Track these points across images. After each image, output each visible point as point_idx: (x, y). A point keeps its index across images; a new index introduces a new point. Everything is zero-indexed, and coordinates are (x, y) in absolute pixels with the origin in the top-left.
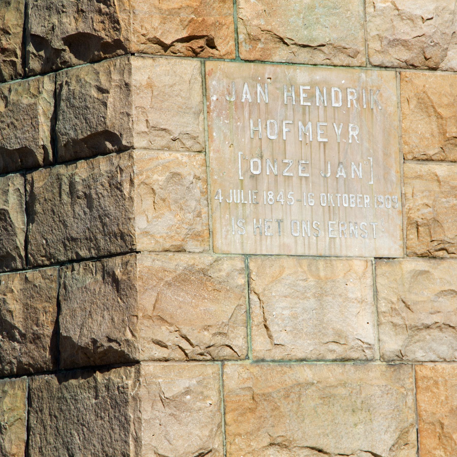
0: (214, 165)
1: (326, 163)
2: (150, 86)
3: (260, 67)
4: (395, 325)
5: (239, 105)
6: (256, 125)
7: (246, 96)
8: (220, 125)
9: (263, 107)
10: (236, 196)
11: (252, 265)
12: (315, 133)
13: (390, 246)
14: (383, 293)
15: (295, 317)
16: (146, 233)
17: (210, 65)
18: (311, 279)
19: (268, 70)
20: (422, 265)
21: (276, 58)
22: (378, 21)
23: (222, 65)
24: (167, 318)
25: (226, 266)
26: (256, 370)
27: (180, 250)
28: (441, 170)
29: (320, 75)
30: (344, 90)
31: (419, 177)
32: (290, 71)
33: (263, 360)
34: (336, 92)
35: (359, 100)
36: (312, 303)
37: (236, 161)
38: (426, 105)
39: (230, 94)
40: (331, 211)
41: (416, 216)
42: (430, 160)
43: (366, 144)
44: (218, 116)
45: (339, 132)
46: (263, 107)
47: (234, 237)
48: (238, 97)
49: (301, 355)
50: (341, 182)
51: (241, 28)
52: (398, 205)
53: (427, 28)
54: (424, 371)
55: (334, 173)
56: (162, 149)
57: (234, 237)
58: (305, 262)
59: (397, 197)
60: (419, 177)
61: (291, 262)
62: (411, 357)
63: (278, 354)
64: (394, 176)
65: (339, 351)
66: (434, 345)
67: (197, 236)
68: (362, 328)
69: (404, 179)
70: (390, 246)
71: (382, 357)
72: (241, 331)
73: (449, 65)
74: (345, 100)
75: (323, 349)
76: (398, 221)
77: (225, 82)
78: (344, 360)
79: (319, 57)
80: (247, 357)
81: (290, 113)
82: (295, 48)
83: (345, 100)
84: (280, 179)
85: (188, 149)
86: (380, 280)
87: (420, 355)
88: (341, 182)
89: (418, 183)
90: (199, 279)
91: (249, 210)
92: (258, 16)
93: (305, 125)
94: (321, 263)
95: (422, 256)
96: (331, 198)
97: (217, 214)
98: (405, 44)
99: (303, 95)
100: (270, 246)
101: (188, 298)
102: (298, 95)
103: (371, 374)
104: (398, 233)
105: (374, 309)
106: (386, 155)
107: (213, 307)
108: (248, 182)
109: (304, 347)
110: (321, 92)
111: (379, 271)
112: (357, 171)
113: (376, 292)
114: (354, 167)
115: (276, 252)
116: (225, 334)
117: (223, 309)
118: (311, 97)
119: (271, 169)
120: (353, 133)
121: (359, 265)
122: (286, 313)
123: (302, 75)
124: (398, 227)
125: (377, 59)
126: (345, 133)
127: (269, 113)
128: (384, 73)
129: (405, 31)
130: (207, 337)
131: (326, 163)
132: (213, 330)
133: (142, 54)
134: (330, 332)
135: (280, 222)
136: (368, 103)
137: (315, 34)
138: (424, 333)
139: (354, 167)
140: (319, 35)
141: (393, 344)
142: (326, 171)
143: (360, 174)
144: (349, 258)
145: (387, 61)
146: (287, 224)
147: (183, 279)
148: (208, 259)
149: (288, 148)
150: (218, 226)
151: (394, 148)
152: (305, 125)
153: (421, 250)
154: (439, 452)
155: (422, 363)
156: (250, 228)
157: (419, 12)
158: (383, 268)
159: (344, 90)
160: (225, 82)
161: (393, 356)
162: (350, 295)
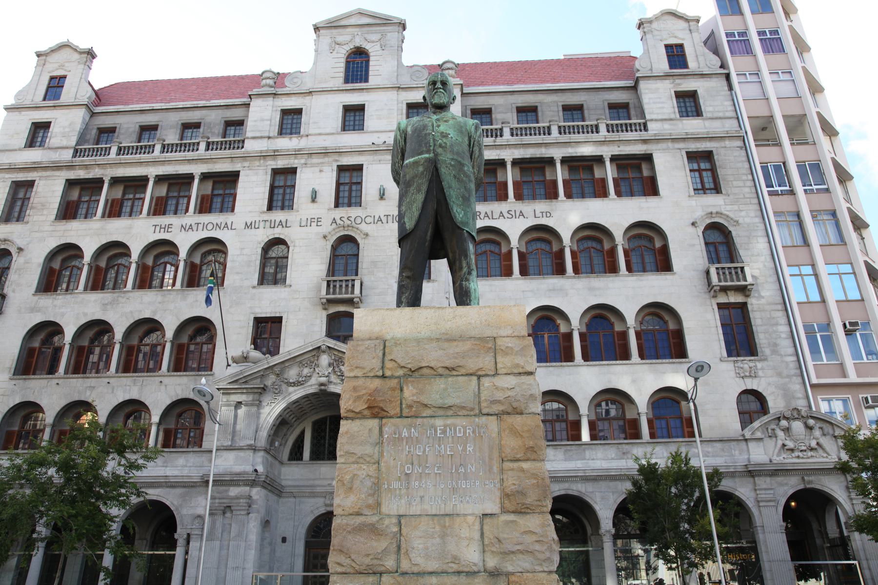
0: (383, 469)
1: (452, 465)
2: (346, 433)
3: (414, 420)
4: (493, 552)
5: (400, 439)
6: (410, 448)
7: (405, 433)
8: (388, 450)
9: (414, 439)
10: (395, 485)
11: (403, 521)
12: (446, 450)
13: (492, 507)
14: (487, 533)
15: (427, 548)
16: (339, 506)
17: (384, 421)
18: (437, 527)
19: (419, 421)
20: (512, 517)
21: (424, 415)
22: (486, 392)
23: (392, 420)
24: (345, 550)
25: (387, 522)
26: (400, 579)
27: (358, 514)
28: (525, 465)
29: (449, 421)
30: (465, 427)
31: (512, 470)
32: (432, 421)
33: (407, 573)
34: (460, 430)
35: (474, 432)
36: (438, 540)
37: (397, 467)
38: (514, 432)
39: (395, 434)
40: (454, 490)
41: (508, 490)
42: (518, 460)
43: (478, 454)
44: (388, 444)
45: (460, 449)
46: (414, 439)
47: (392, 506)
48: (400, 435)
49: (430, 570)
50: (462, 474)
51: (404, 401)
52: (498, 485)
53: (509, 393)
54: (512, 578)
55: (457, 470)
56: (353, 463)
57: (392, 506)
58: (436, 518)
59: (497, 480)
60: (512, 470)
61: (426, 518)
62: (505, 570)
63: (416, 569)
64: (495, 469)
65: (455, 567)
66: (520, 563)
67: (369, 506)
68: (472, 555)
69: (502, 471)
70: (492, 507)
71: (485, 571)
72: (394, 556)
73: (530, 411)
74: (465, 432)
75: (445, 567)
76: (498, 494)
77: (393, 428)
78: (459, 573)
79: (450, 413)
80: (397, 572)
81: (431, 441)
82: (434, 409)
83: (465, 432)
84: (423, 475)
85: (369, 462)
86: (485, 527)
87: (510, 569)
88: (462, 474)
89: (510, 473)
90: (374, 530)
91: (404, 491)
92: (413, 395)
93: (440, 446)
94: (447, 519)
95: (513, 512)
96: (454, 483)
97: (383, 495)
98: (499, 402)
99: (439, 432)
100: (415, 509)
101: (362, 540)
102: (436, 431)
103: (476, 581)
104: (498, 500)
105: (481, 543)
106: (491, 459)
107: (375, 544)
108: (403, 477)
109: (433, 566)
110: (450, 429)
111: (485, 522)
112: (471, 468)
113: (482, 534)
114: (470, 466)
115: (418, 513)
116: (380, 559)
117: (381, 545)
118: (444, 432)
119: (418, 470)
120: (470, 449)
121: (470, 519)
122: (421, 546)
123: (439, 422)
124: (56, 302)
125: (485, 411)
126: (465, 449)
127: (418, 441)
128: (490, 417)
129: (500, 396)
130: (367, 561)
131: (452, 465)
132: (371, 557)
133: (347, 418)
134: (450, 556)
135: (422, 497)
136: (479, 433)
137: (446, 401)
138: (512, 556)
139: (470, 466)
140: (449, 402)
141: (492, 562)
142: (452, 469)
143: (473, 470)
144: (466, 515)
145: (491, 411)
146: (426, 498)
147: (359, 529)
148: (375, 519)
149: (429, 458)
150: (383, 501)
151: (496, 455)
152: (440, 446)
153: (512, 508)
154: (6, 463)
155: (513, 574)
156: (403, 501)
157: (506, 386)
158: (487, 520)
159: (465, 427)
160: (393, 428)
161: (492, 570)
162: (463, 536)
